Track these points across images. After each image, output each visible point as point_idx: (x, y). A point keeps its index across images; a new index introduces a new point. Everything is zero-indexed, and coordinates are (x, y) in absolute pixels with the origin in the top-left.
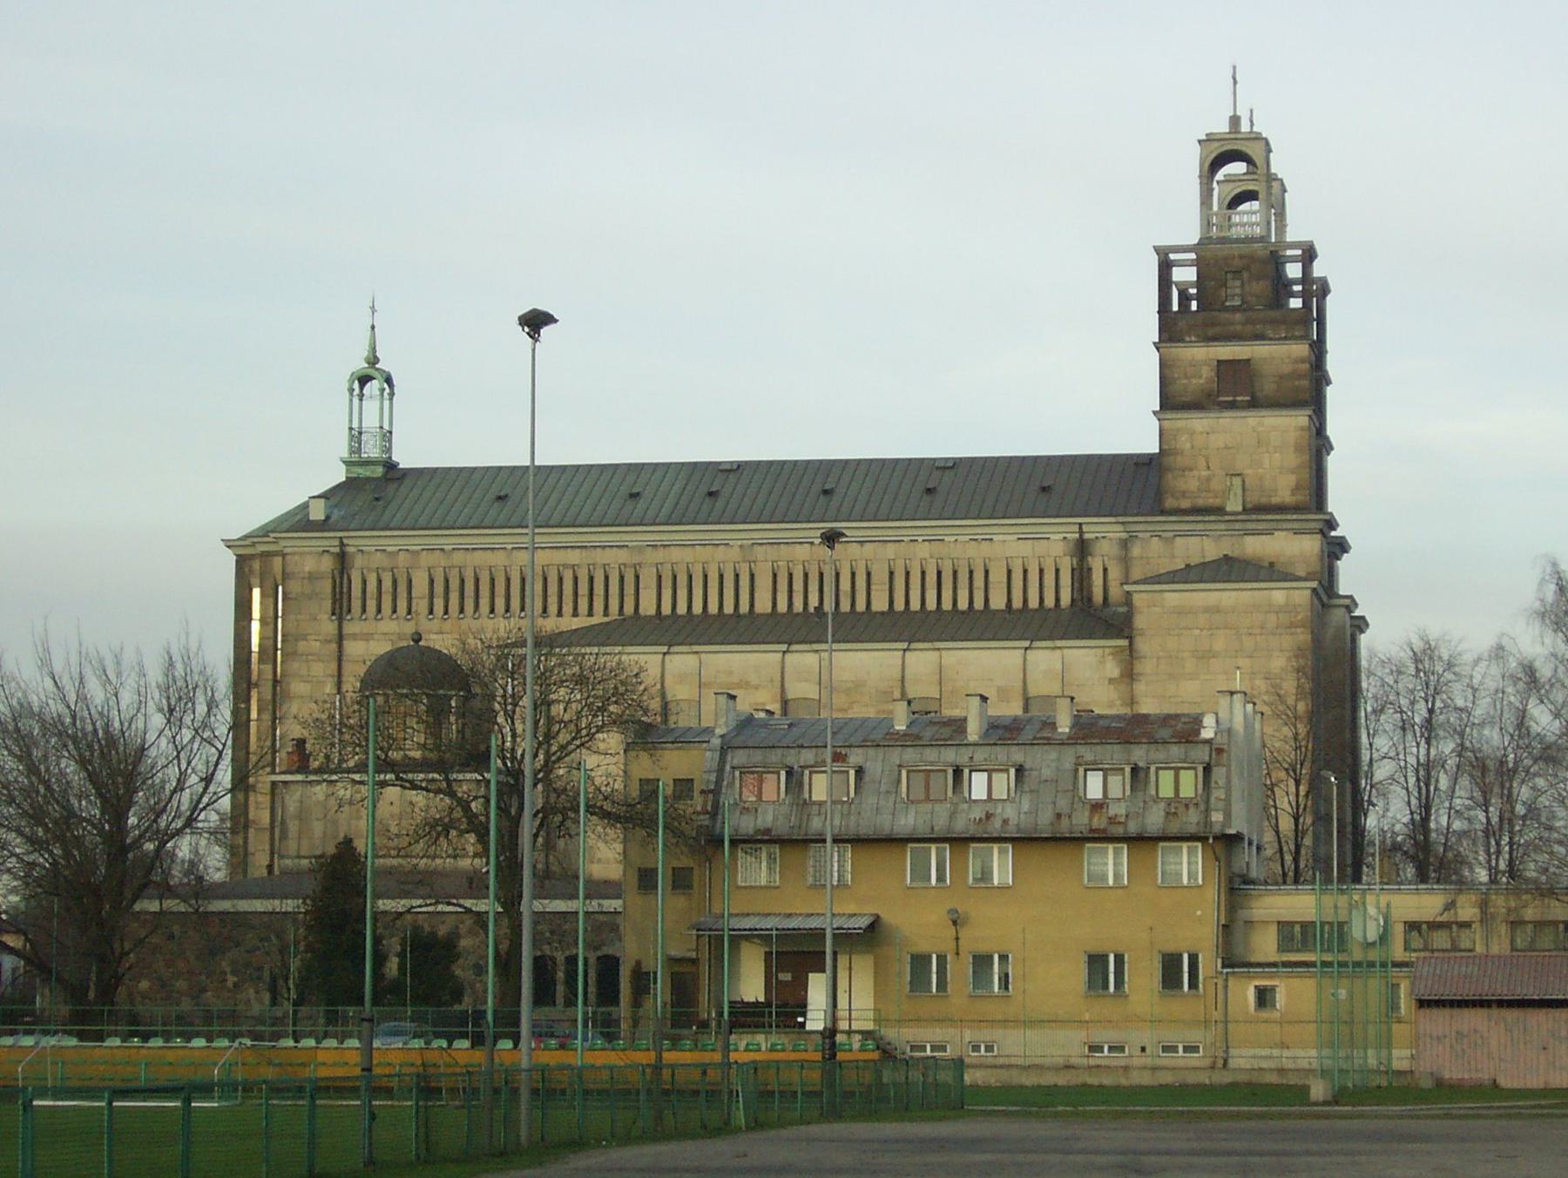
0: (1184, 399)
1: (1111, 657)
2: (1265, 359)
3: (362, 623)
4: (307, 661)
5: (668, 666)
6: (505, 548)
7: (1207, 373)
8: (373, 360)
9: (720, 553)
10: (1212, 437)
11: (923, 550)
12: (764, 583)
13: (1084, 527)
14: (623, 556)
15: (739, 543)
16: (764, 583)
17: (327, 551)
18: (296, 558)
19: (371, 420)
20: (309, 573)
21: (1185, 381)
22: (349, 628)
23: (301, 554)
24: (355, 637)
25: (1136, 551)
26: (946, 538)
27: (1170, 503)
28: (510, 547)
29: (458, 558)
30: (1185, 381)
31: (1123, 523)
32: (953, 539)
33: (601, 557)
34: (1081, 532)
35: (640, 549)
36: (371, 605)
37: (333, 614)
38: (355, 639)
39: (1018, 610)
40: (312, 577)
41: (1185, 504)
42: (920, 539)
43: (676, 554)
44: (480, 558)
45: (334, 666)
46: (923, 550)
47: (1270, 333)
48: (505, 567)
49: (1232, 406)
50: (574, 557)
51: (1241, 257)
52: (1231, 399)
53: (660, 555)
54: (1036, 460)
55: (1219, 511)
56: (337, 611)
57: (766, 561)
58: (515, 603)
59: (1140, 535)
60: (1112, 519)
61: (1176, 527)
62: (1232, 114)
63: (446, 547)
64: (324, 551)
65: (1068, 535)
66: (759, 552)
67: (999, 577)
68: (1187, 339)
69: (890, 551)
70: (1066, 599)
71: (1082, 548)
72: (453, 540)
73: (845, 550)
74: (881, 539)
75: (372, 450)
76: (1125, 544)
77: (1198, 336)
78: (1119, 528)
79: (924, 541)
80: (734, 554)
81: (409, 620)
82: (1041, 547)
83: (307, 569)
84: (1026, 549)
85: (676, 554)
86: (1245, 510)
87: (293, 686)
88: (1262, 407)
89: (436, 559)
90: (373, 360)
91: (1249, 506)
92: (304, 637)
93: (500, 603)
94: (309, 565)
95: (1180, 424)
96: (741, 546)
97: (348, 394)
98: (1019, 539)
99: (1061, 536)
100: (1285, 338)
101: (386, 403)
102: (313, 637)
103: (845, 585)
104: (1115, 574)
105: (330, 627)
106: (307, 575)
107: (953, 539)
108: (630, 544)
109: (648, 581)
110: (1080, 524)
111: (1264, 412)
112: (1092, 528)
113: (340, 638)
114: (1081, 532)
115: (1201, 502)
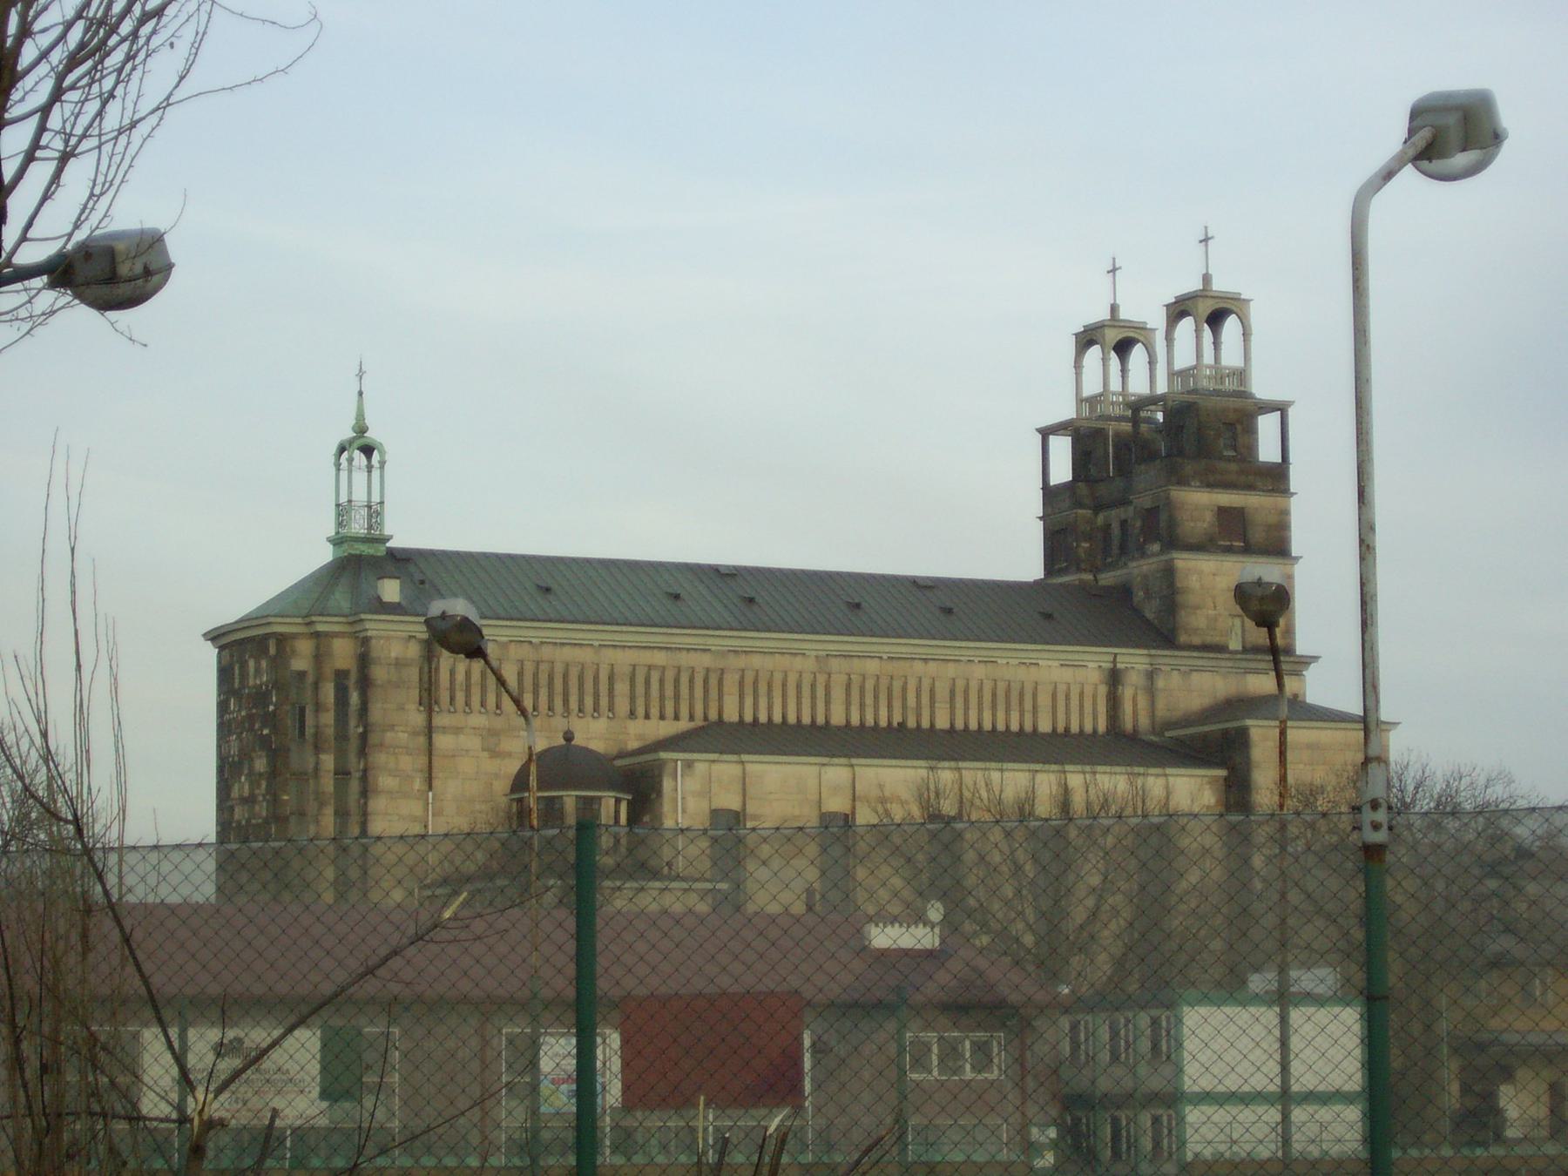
0: (1191, 541)
1: (1208, 787)
2: (1257, 509)
3: (452, 715)
4: (394, 754)
5: (824, 777)
6: (592, 645)
7: (1209, 517)
8: (361, 430)
9: (798, 663)
10: (1218, 579)
11: (979, 672)
12: (838, 694)
13: (1118, 657)
14: (706, 660)
15: (814, 653)
16: (838, 694)
17: (414, 637)
18: (382, 642)
19: (360, 496)
20: (397, 659)
21: (1192, 524)
22: (438, 720)
23: (388, 638)
24: (444, 730)
25: (1160, 683)
26: (999, 661)
27: (1183, 638)
28: (596, 643)
29: (546, 652)
30: (1192, 524)
31: (1150, 656)
32: (1004, 661)
33: (685, 660)
34: (1114, 662)
35: (724, 654)
36: (460, 697)
37: (420, 704)
38: (444, 733)
39: (942, 730)
40: (399, 664)
41: (1196, 641)
42: (976, 660)
43: (756, 661)
44: (568, 654)
45: (423, 760)
46: (979, 672)
47: (1259, 484)
48: (1009, 682)
49: (1229, 550)
50: (659, 658)
51: (1236, 410)
52: (1228, 543)
53: (741, 662)
54: (961, 581)
55: (1220, 649)
56: (425, 700)
57: (840, 673)
58: (604, 702)
59: (1163, 668)
60: (1145, 652)
61: (1190, 662)
62: (1204, 272)
63: (534, 640)
64: (410, 637)
65: (1103, 664)
66: (835, 664)
67: (1044, 700)
68: (1193, 484)
69: (951, 670)
70: (1102, 727)
71: (1114, 678)
72: (542, 634)
73: (911, 667)
74: (942, 657)
75: (358, 527)
76: (1151, 675)
77: (1201, 482)
78: (1147, 660)
79: (979, 662)
80: (809, 665)
81: (536, 716)
82: (1080, 673)
83: (393, 655)
84: (1067, 675)
85: (756, 661)
86: (1245, 650)
87: (380, 779)
88: (1254, 553)
89: (525, 652)
90: (361, 430)
91: (1248, 646)
92: (392, 727)
93: (589, 701)
94: (395, 650)
95: (1191, 564)
96: (817, 657)
97: (334, 469)
98: (1062, 665)
99: (1096, 665)
100: (1273, 490)
101: (344, 475)
102: (401, 728)
103: (911, 701)
104: (1142, 702)
105: (417, 718)
106: (394, 662)
107: (1004, 661)
108: (713, 648)
109: (731, 682)
110: (1116, 655)
111: (1253, 559)
112: (1127, 659)
113: (429, 730)
114: (1114, 662)
115: (1209, 640)
